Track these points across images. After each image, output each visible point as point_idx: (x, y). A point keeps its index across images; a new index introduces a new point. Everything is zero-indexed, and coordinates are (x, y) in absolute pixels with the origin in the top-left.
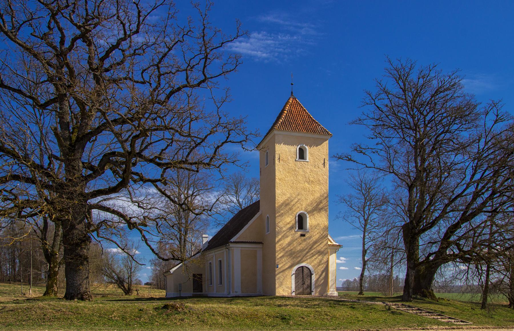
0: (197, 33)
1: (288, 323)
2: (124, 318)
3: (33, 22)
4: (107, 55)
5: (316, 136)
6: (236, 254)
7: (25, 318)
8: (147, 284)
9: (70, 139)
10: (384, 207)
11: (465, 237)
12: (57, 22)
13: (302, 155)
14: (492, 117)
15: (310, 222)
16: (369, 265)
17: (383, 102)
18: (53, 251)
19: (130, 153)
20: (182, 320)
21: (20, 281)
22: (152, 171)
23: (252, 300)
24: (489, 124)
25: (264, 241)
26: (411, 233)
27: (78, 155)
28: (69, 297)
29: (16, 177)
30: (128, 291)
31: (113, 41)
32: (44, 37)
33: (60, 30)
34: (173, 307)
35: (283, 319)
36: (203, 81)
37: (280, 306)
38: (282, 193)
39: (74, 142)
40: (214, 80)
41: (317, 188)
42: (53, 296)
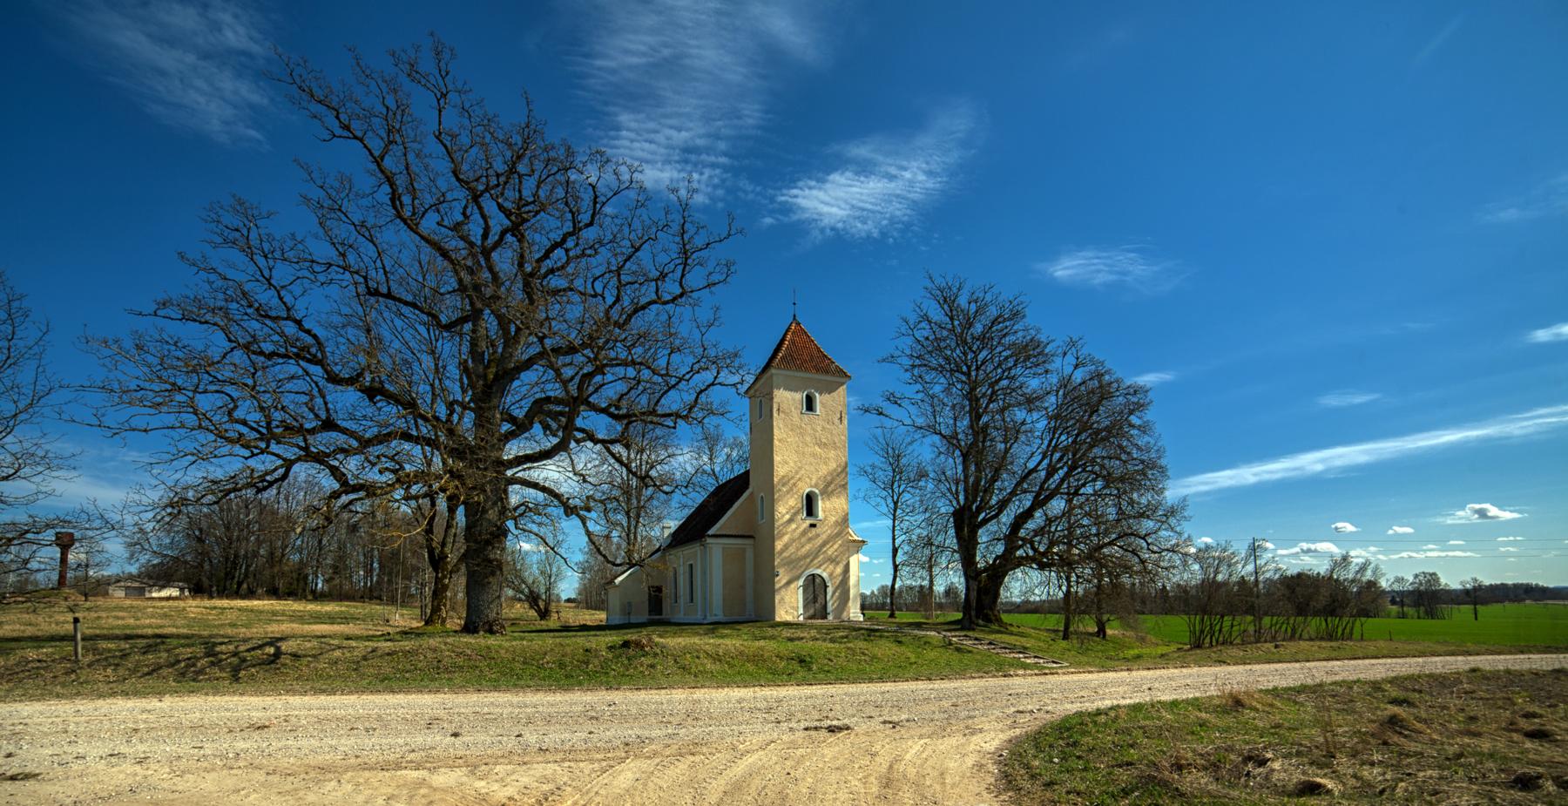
0: (676, 228)
1: (810, 669)
2: (562, 665)
3: (441, 207)
4: (546, 256)
5: (829, 378)
6: (715, 555)
7: (408, 667)
8: (569, 600)
9: (485, 377)
10: (922, 483)
11: (1040, 532)
12: (480, 208)
13: (810, 405)
14: (1070, 359)
15: (821, 506)
16: (904, 571)
17: (924, 332)
18: (442, 552)
19: (575, 399)
20: (652, 666)
21: (380, 598)
22: (602, 425)
23: (745, 629)
24: (1068, 370)
25: (758, 535)
26: (966, 523)
27: (495, 401)
28: (469, 628)
29: (406, 436)
30: (544, 614)
31: (556, 236)
32: (456, 227)
33: (484, 217)
34: (638, 645)
35: (802, 661)
36: (681, 295)
37: (791, 640)
38: (785, 460)
39: (489, 380)
40: (695, 295)
41: (832, 454)
42: (439, 626)
